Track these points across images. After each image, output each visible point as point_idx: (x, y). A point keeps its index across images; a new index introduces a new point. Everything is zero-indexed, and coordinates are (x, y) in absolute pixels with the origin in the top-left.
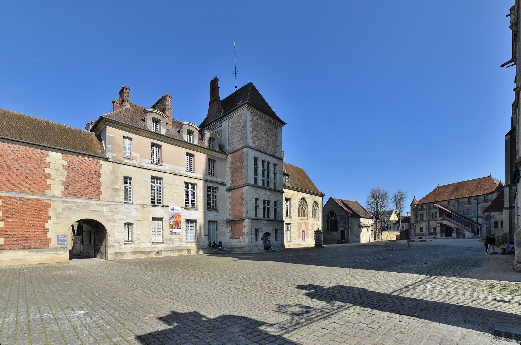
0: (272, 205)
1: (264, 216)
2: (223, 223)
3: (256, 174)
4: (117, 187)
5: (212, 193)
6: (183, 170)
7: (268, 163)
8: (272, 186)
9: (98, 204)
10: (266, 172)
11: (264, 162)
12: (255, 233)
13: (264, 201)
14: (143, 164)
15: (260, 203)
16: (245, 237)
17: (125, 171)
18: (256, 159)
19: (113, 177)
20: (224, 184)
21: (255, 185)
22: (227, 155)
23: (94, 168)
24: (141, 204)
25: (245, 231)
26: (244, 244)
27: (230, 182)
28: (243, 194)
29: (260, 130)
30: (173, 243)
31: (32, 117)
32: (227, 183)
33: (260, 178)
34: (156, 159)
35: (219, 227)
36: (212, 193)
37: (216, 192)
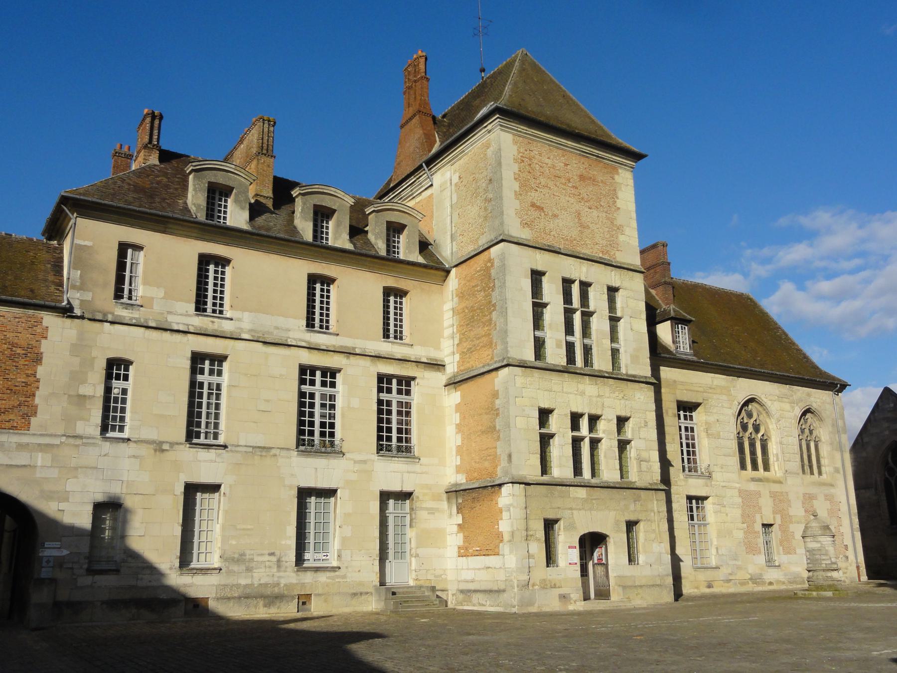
0: (606, 429)
1: (578, 470)
2: (436, 498)
3: (538, 322)
4: (85, 390)
5: (394, 397)
6: (294, 326)
7: (585, 286)
8: (602, 362)
9: (21, 447)
10: (577, 318)
11: (567, 283)
12: (541, 534)
13: (575, 418)
14: (170, 318)
15: (559, 424)
16: (505, 548)
17: (113, 341)
18: (537, 276)
19: (76, 361)
20: (436, 366)
21: (538, 361)
22: (448, 272)
23: (24, 338)
24: (152, 442)
25: (504, 526)
26: (501, 576)
27: (457, 357)
28: (495, 395)
29: (551, 184)
30: (249, 570)
31: (24, 237)
32: (447, 361)
33: (554, 335)
34: (315, 316)
35: (422, 515)
36: (394, 397)
37: (408, 393)
